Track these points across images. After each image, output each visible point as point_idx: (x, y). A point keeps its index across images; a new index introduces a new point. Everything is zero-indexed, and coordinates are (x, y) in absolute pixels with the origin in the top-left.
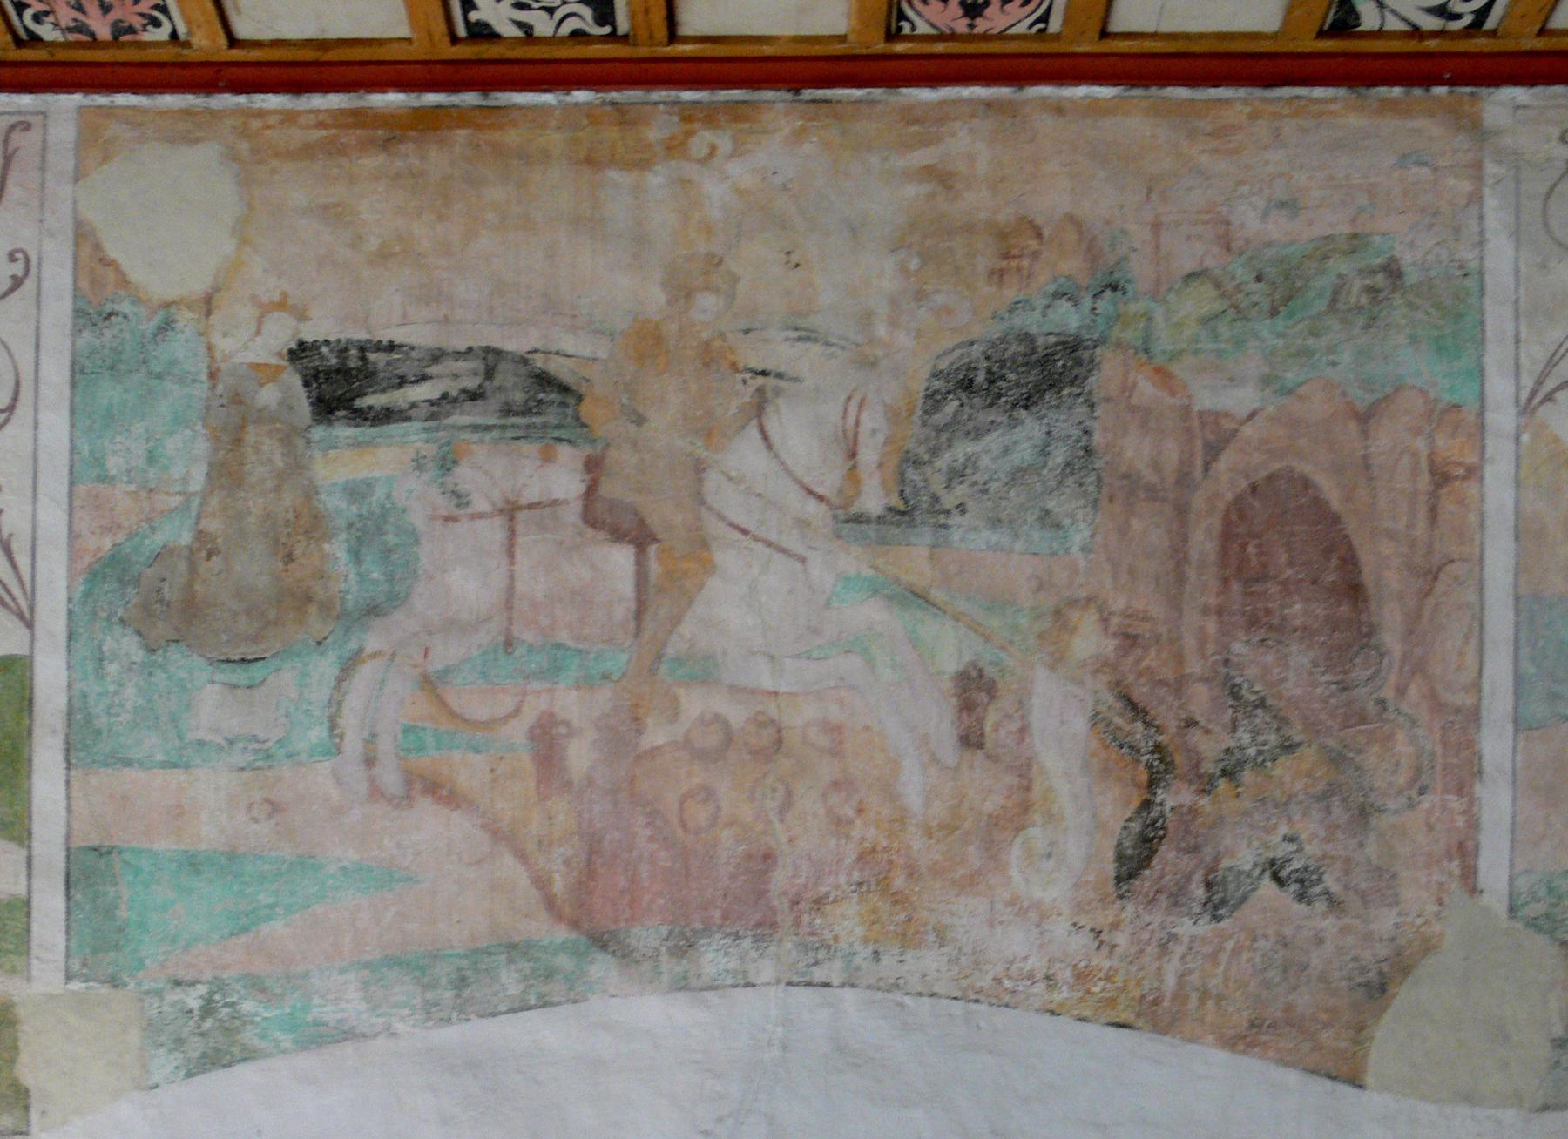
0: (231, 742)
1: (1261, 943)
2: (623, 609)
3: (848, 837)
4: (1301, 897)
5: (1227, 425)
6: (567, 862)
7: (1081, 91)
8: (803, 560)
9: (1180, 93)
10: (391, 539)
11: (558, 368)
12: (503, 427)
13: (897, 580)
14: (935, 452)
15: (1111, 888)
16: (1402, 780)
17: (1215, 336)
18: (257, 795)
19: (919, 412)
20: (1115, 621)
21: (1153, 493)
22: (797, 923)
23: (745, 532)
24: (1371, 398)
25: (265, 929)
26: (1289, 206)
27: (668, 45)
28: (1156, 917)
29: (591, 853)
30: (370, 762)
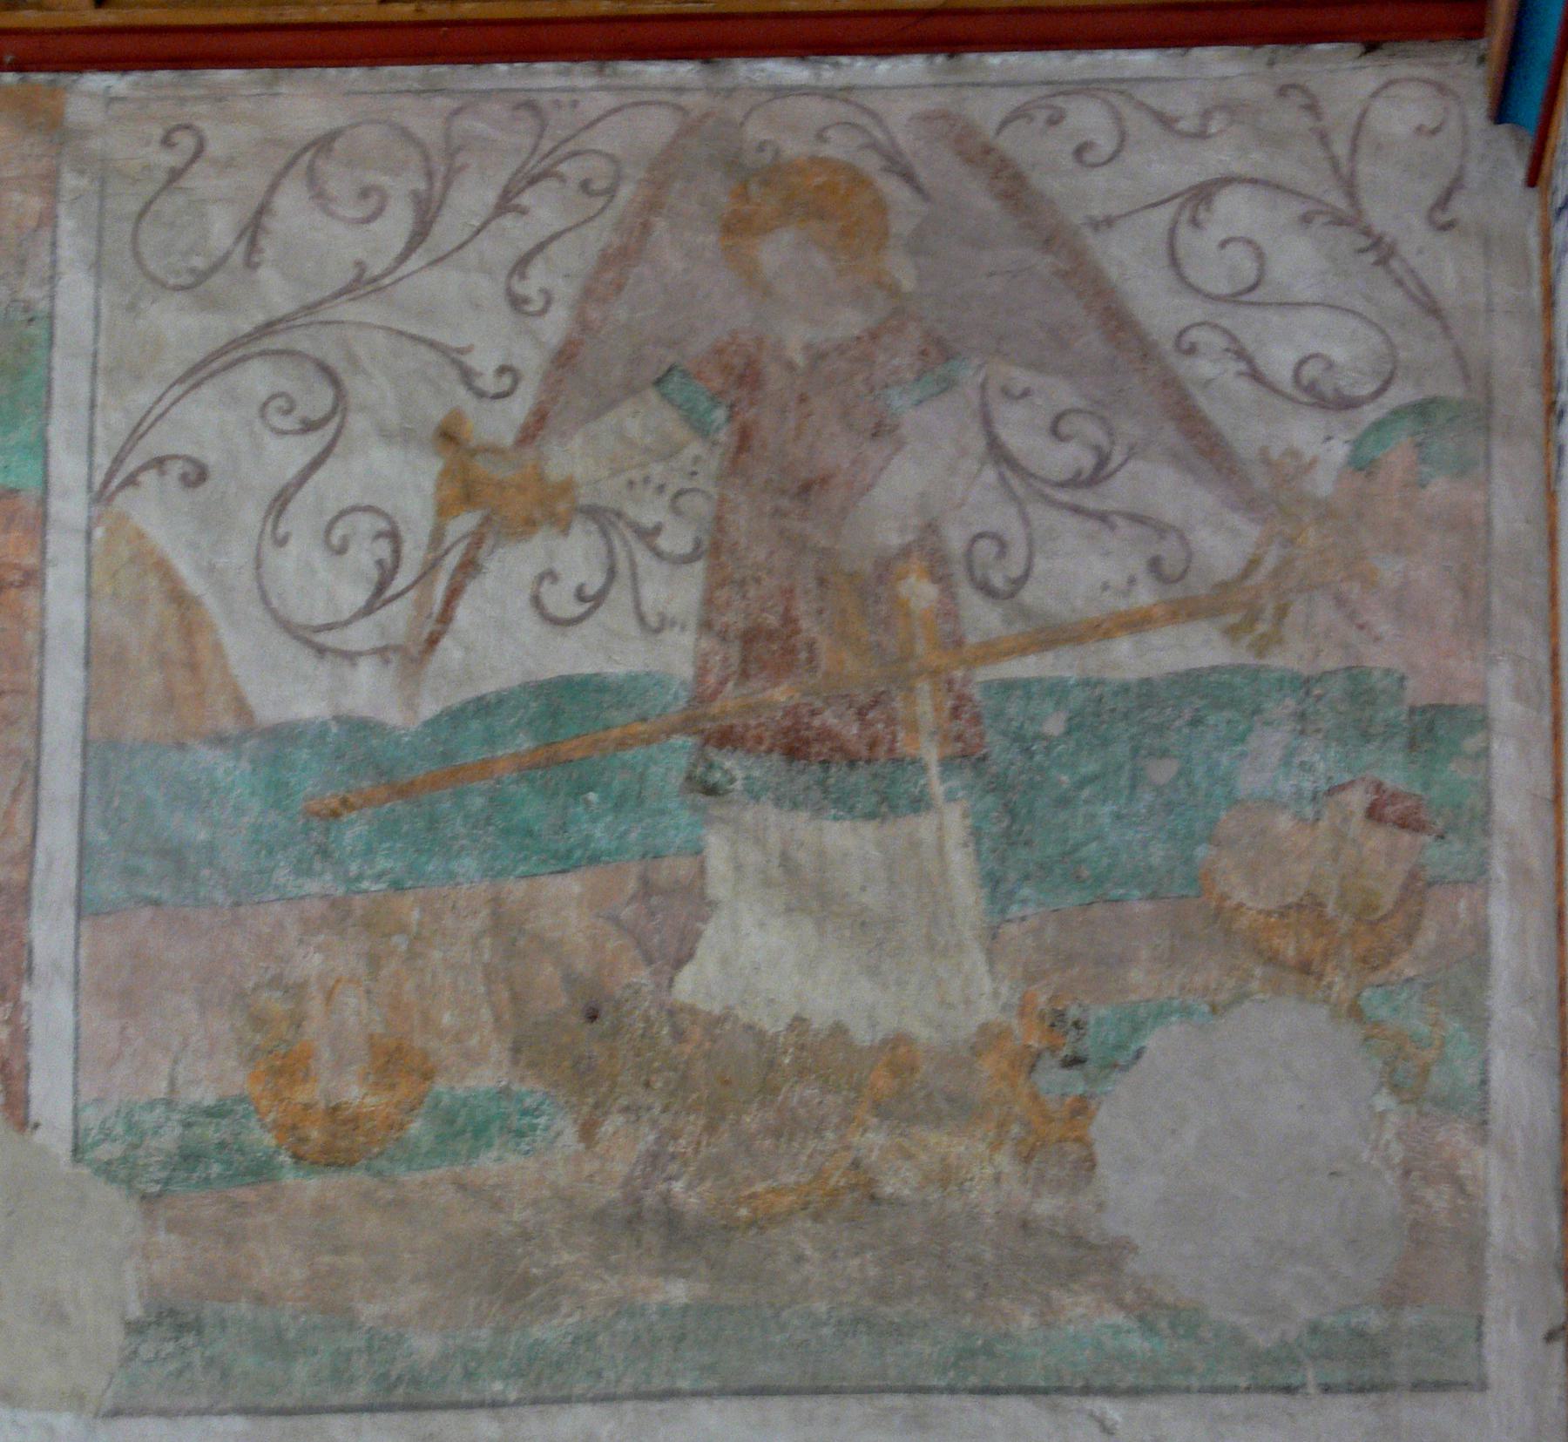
27: (765, 141)
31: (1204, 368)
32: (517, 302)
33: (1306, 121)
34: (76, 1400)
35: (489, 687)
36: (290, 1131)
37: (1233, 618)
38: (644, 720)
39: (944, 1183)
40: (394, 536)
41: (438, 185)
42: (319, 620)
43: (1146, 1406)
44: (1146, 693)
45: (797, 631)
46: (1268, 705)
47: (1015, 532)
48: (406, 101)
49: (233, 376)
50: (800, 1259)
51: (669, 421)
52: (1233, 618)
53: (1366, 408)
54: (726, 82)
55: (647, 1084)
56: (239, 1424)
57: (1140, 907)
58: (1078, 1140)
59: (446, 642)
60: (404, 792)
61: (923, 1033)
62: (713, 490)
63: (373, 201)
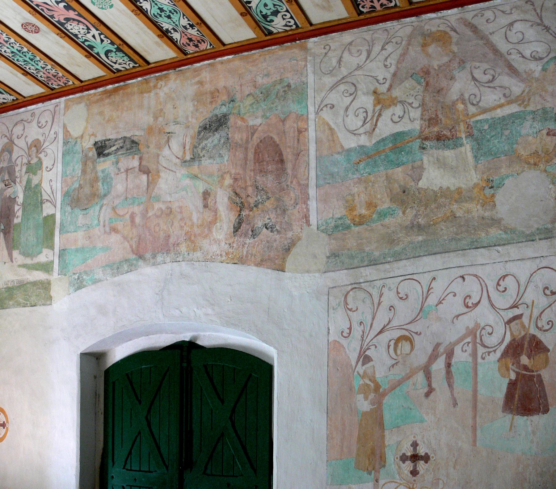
0: (83, 226)
1: (264, 243)
2: (145, 189)
3: (183, 230)
4: (272, 231)
5: (255, 128)
6: (135, 242)
7: (226, 58)
8: (175, 172)
9: (246, 53)
10: (108, 180)
11: (135, 139)
12: (126, 153)
13: (192, 174)
14: (199, 144)
15: (232, 234)
16: (292, 202)
17: (253, 108)
18: (87, 236)
19: (197, 136)
20: (233, 176)
21: (241, 146)
22: (174, 249)
23: (165, 168)
24: (284, 116)
25: (88, 262)
26: (267, 75)
28: (242, 239)
29: (140, 239)
30: (104, 226)
31: (513, 57)
32: (386, 66)
33: (532, 7)
34: (319, 271)
35: (384, 136)
36: (353, 220)
37: (520, 102)
38: (411, 138)
39: (468, 213)
40: (366, 112)
41: (371, 47)
42: (354, 129)
43: (506, 247)
44: (503, 118)
45: (438, 117)
46: (527, 117)
47: (478, 93)
48: (365, 33)
49: (337, 88)
50: (442, 230)
51: (414, 83)
52: (520, 102)
53: (545, 59)
54: (421, 19)
55: (414, 203)
56: (346, 271)
57: (503, 158)
58: (493, 201)
59: (376, 129)
60: (369, 157)
61: (463, 186)
62: (422, 94)
63: (360, 52)
